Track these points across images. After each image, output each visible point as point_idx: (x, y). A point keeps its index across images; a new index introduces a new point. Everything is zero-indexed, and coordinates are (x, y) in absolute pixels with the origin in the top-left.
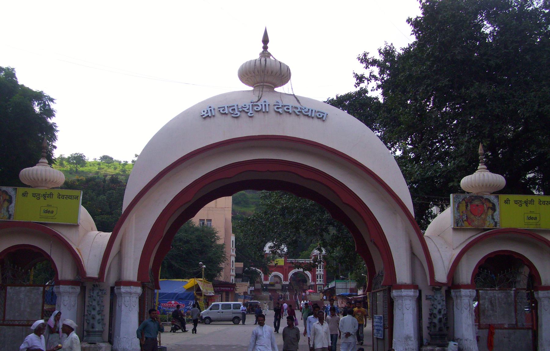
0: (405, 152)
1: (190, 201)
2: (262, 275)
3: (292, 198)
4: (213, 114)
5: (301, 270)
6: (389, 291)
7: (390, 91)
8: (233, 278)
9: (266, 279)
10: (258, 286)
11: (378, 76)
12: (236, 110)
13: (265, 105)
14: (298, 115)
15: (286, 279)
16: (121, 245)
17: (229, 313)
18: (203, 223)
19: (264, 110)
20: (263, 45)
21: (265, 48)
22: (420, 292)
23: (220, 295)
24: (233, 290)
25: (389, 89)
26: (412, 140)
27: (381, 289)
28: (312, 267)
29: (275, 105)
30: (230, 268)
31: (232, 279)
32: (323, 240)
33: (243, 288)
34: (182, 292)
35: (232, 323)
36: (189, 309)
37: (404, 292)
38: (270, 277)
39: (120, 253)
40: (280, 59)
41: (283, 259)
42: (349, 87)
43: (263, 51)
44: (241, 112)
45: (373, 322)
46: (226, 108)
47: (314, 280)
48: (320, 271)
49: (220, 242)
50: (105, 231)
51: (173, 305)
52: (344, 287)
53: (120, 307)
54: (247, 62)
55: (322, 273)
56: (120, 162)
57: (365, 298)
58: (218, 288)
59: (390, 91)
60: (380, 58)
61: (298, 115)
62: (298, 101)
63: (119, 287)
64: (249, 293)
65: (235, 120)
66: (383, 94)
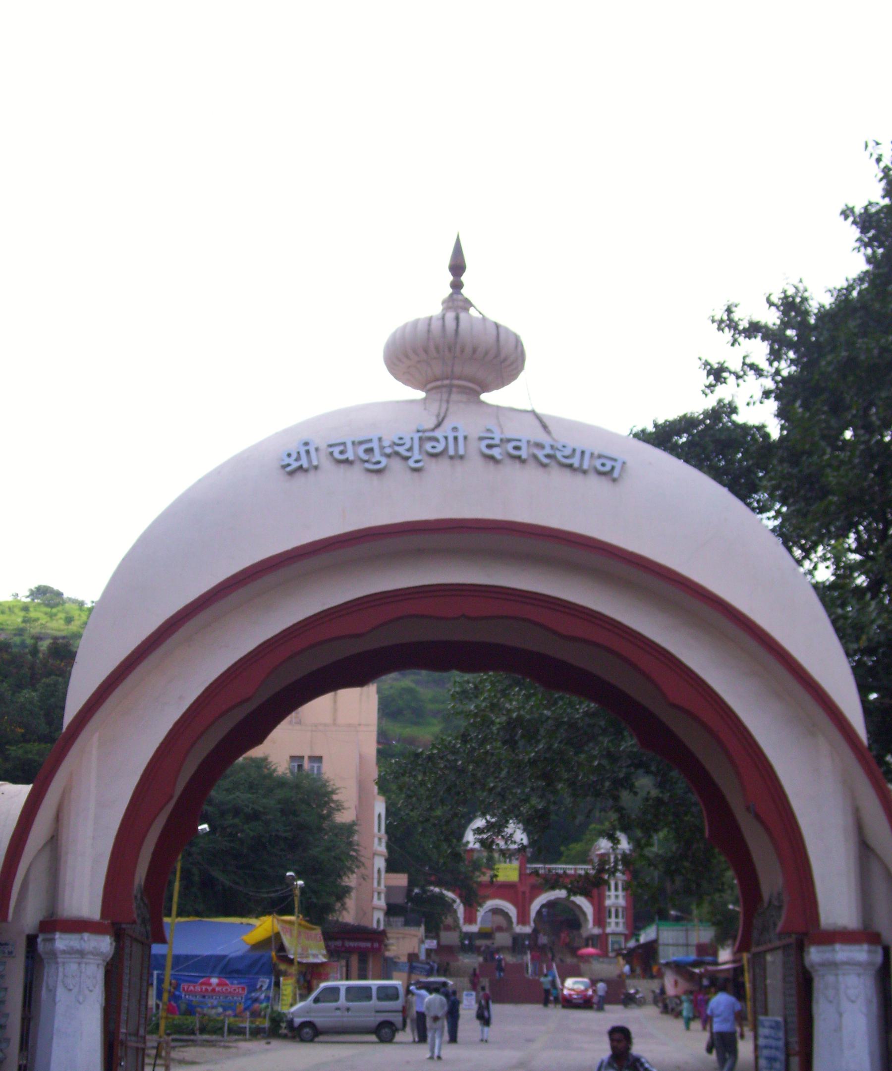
0: (844, 572)
1: (247, 700)
2: (460, 909)
3: (534, 695)
4: (315, 463)
5: (561, 893)
6: (800, 949)
7: (798, 404)
8: (379, 915)
9: (470, 919)
10: (449, 938)
11: (764, 365)
12: (377, 451)
13: (456, 439)
14: (544, 466)
15: (523, 918)
16: (58, 818)
17: (368, 1012)
18: (300, 767)
19: (451, 452)
20: (450, 278)
21: (457, 286)
22: (886, 950)
23: (343, 962)
24: (379, 950)
25: (794, 401)
26: (858, 539)
27: (777, 943)
28: (592, 886)
29: (481, 439)
30: (371, 888)
31: (377, 919)
32: (620, 810)
33: (408, 941)
34: (239, 953)
35: (374, 1038)
36: (256, 1000)
37: (842, 953)
38: (481, 913)
39: (54, 842)
40: (495, 315)
41: (516, 864)
42: (693, 401)
43: (451, 295)
44: (388, 456)
45: (756, 1038)
46: (349, 446)
47: (600, 921)
48: (615, 898)
49: (344, 817)
50: (15, 781)
51: (214, 990)
52: (682, 941)
53: (52, 992)
54: (405, 326)
55: (622, 902)
56: (81, 604)
57: (738, 971)
58: (339, 943)
59: (798, 404)
60: (771, 318)
61: (544, 466)
62: (545, 427)
63: (49, 936)
64: (423, 956)
65: (375, 478)
66: (781, 414)
